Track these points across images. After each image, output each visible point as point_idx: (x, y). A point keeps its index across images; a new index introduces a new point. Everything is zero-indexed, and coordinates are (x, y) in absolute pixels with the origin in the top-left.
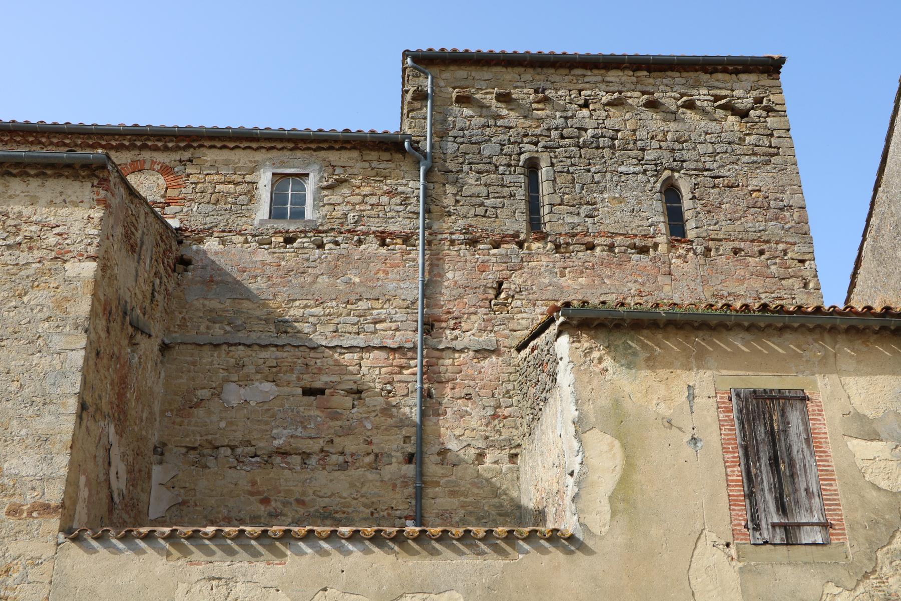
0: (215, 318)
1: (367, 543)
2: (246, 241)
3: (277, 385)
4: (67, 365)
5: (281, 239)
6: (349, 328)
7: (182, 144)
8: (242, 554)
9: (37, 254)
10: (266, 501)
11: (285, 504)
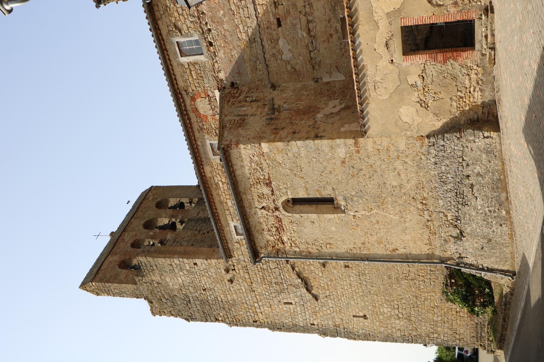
0: (255, 69)
1: (355, 36)
2: (216, 62)
3: (279, 39)
4: (303, 146)
5: (211, 48)
6: (246, 12)
7: (180, 96)
8: (365, 79)
9: (263, 162)
10: (331, 35)
11: (331, 27)
